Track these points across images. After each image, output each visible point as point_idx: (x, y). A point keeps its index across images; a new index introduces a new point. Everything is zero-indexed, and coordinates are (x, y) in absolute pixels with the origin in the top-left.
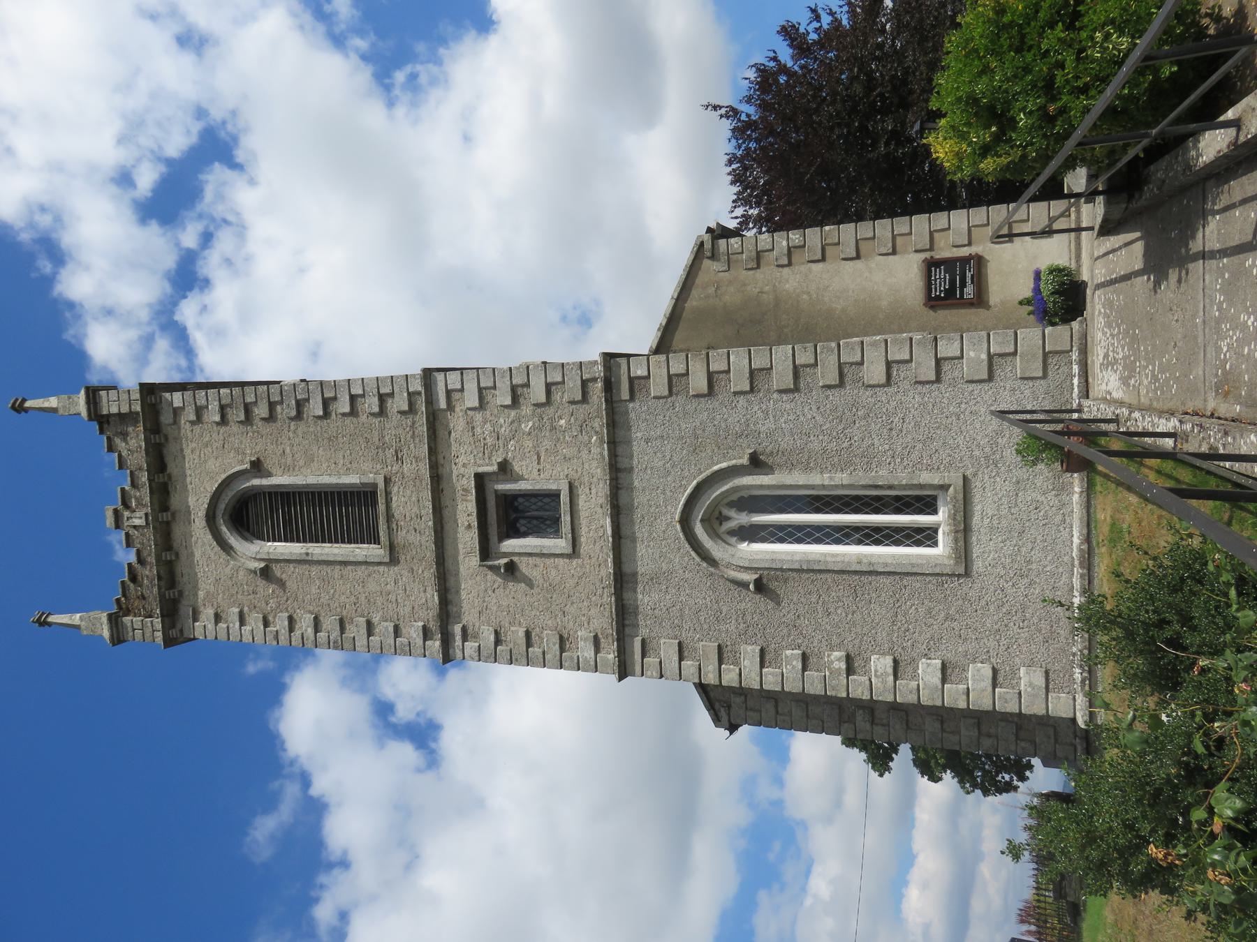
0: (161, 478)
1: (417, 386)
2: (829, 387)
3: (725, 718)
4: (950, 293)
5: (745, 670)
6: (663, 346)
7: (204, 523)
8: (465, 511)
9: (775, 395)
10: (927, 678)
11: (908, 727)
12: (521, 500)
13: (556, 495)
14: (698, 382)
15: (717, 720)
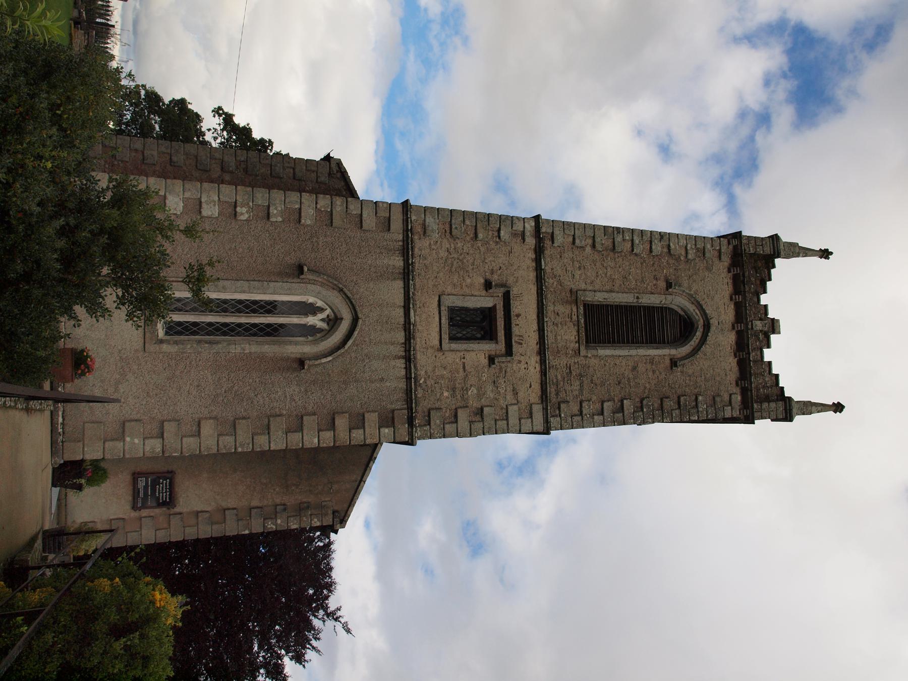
0: (743, 355)
1: (554, 421)
2: (244, 418)
3: (333, 165)
4: (155, 483)
5: (310, 207)
6: (374, 449)
7: (711, 321)
8: (525, 326)
9: (285, 412)
10: (176, 200)
11: (196, 157)
12: (479, 336)
13: (453, 338)
14: (342, 423)
15: (339, 163)
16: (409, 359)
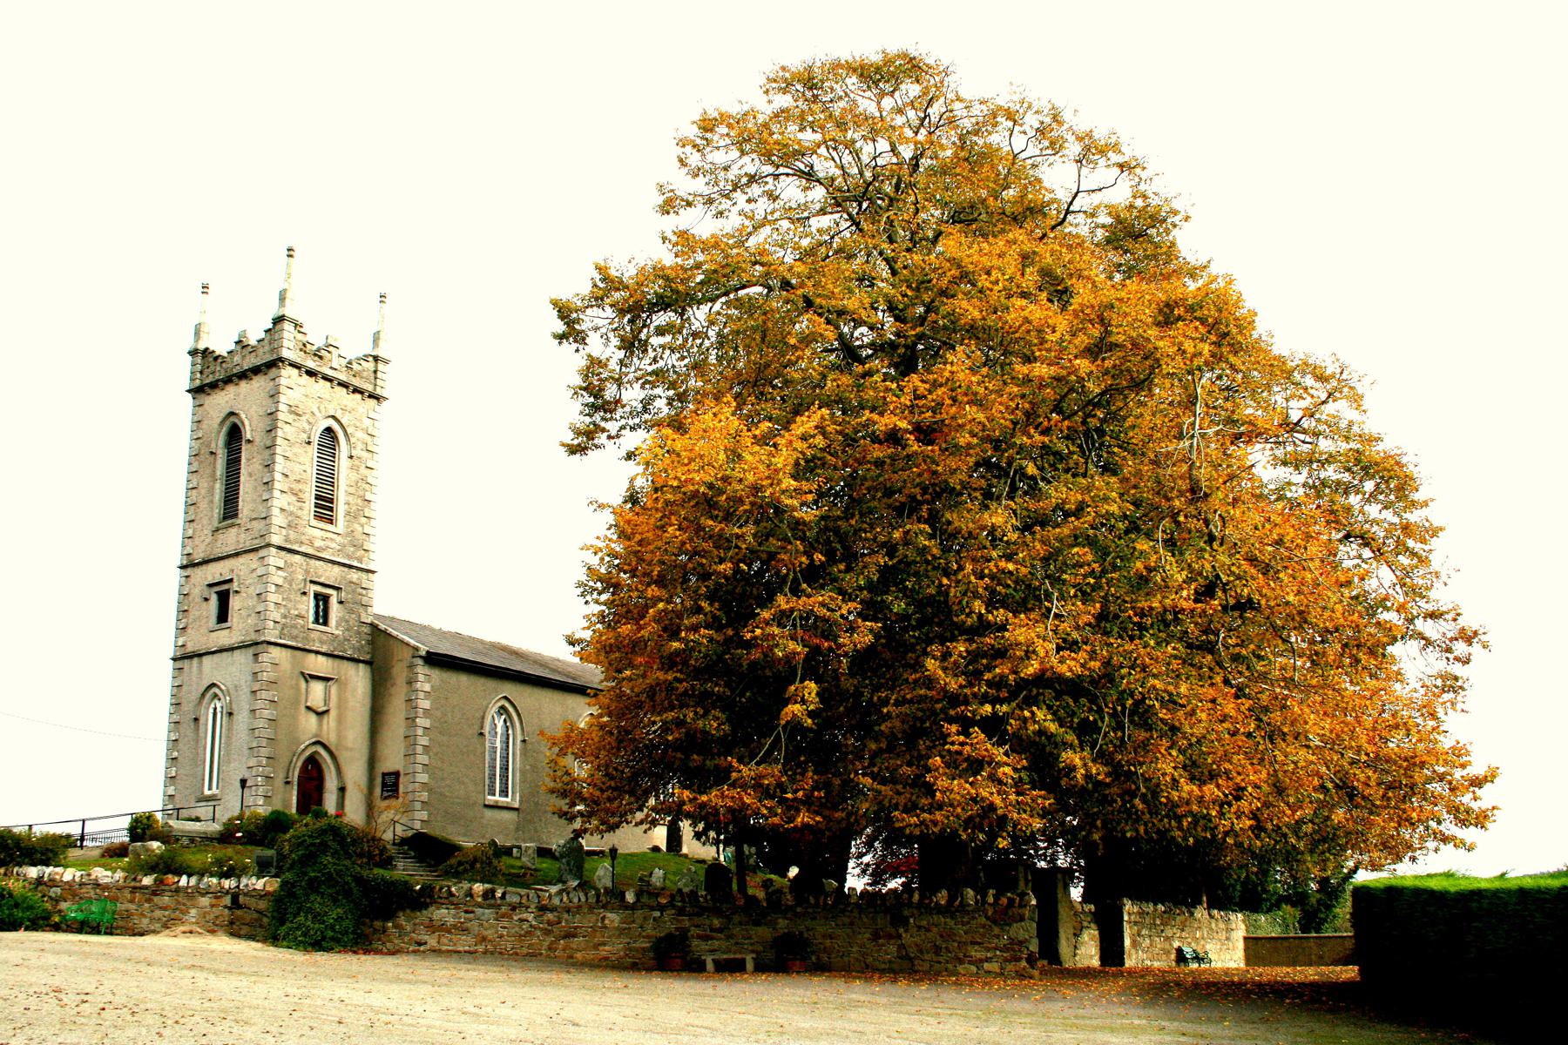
16: (231, 649)
